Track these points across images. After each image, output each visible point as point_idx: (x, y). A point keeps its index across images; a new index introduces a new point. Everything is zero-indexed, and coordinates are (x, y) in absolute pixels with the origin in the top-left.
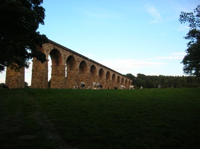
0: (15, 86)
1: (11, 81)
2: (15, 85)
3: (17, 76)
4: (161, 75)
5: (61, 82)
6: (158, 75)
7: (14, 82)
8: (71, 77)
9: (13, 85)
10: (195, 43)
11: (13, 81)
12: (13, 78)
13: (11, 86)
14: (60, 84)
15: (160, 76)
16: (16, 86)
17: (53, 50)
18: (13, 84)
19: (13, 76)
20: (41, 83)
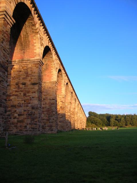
0: (26, 127)
1: (16, 115)
2: (25, 124)
3: (30, 105)
4: (108, 113)
5: (62, 119)
6: (105, 113)
7: (21, 118)
8: (27, 103)
9: (19, 124)
10: (90, 118)
11: (19, 115)
12: (18, 110)
13: (16, 126)
14: (60, 122)
15: (106, 114)
16: (28, 126)
17: (19, 3)
18: (22, 121)
19: (20, 106)
20: (48, 120)
